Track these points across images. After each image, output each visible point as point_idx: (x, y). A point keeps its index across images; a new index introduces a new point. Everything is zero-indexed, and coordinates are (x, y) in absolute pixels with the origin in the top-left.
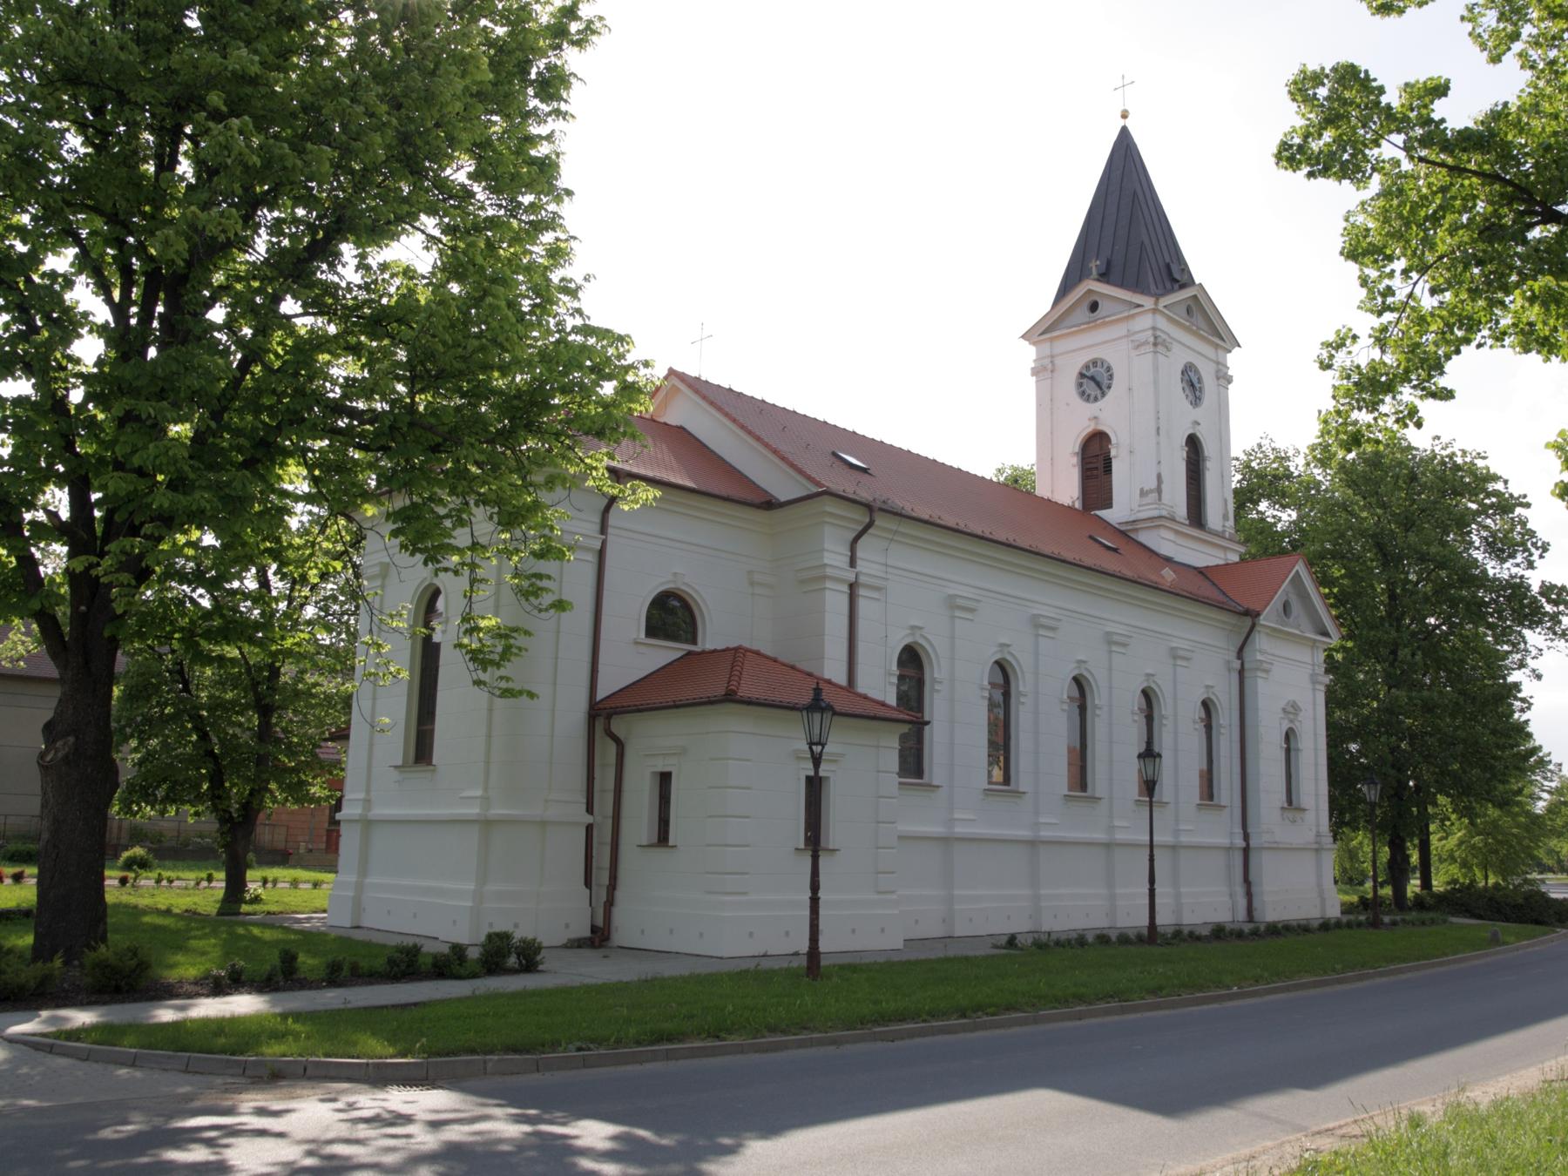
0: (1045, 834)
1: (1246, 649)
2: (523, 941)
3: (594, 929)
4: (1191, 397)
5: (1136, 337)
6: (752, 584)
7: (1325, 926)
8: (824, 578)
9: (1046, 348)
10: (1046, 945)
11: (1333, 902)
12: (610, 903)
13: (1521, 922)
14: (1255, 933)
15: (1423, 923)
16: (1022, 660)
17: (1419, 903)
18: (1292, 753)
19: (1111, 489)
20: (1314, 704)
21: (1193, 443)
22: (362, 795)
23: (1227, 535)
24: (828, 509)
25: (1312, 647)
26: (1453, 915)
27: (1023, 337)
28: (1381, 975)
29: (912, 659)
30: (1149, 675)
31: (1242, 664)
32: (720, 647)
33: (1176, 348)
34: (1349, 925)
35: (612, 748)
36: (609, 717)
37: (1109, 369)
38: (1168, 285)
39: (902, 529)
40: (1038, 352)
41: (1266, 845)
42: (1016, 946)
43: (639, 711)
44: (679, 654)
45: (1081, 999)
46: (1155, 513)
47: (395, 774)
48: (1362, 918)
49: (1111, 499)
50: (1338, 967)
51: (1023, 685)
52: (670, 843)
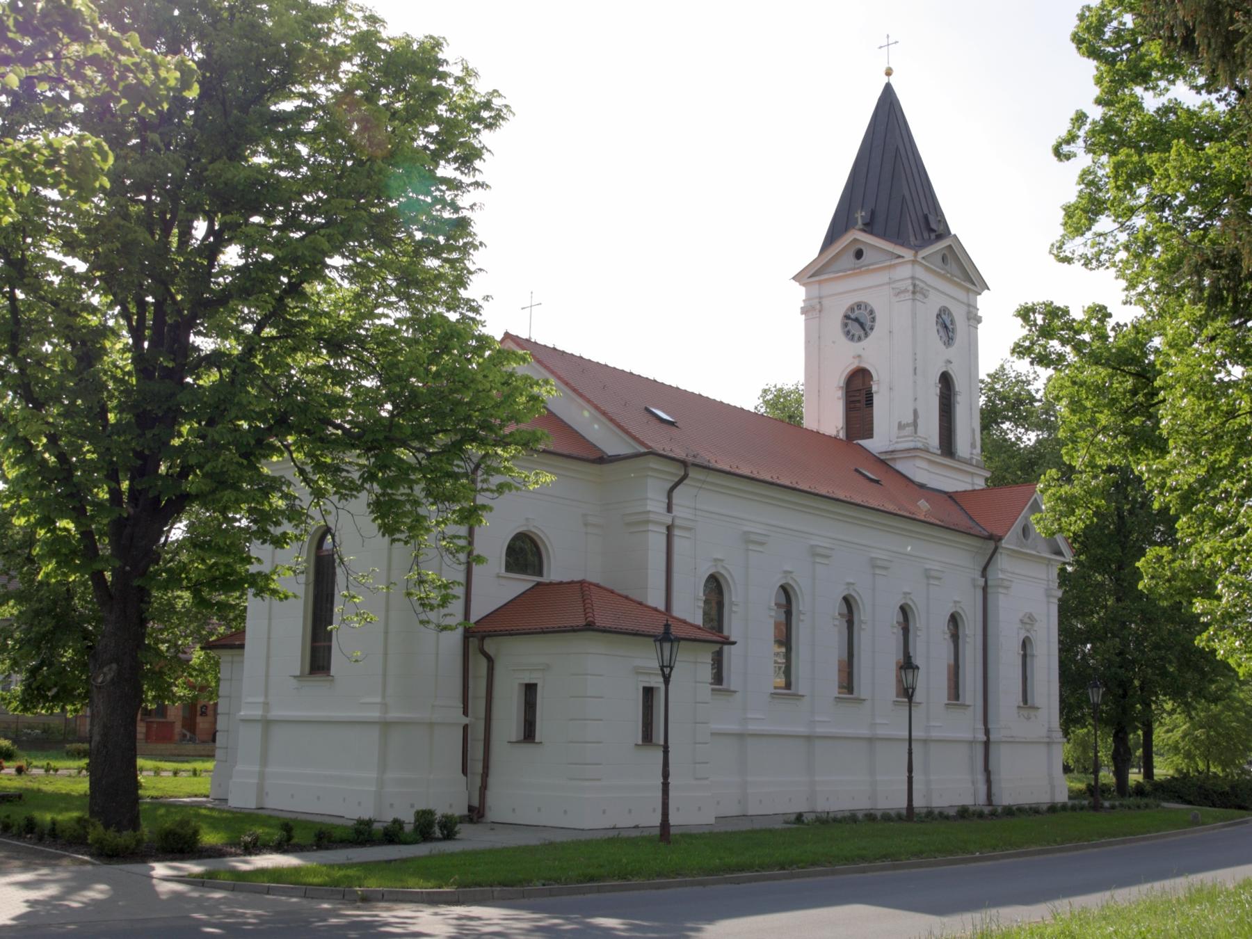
0: (820, 730)
1: (990, 569)
2: (1104, 785)
3: (471, 809)
4: (945, 338)
5: (894, 286)
6: (586, 525)
7: (1053, 809)
8: (647, 522)
9: (815, 290)
10: (826, 822)
11: (1062, 788)
12: (484, 787)
13: (1226, 807)
14: (993, 814)
15: (1139, 807)
16: (802, 586)
17: (1139, 791)
18: (1028, 659)
19: (872, 423)
20: (1048, 616)
21: (946, 380)
22: (261, 699)
23: (974, 462)
24: (652, 465)
25: (1048, 565)
26: (1168, 801)
27: (794, 278)
28: (1094, 846)
29: (715, 586)
30: (906, 594)
31: (986, 582)
32: (566, 580)
33: (933, 295)
34: (1073, 808)
35: (483, 663)
36: (482, 639)
37: (872, 312)
38: (926, 235)
39: (708, 479)
40: (807, 292)
41: (1004, 739)
42: (803, 822)
43: (511, 635)
44: (530, 585)
45: (863, 859)
46: (911, 445)
47: (294, 682)
48: (1085, 802)
49: (872, 429)
50: (1058, 839)
51: (802, 605)
52: (537, 740)
